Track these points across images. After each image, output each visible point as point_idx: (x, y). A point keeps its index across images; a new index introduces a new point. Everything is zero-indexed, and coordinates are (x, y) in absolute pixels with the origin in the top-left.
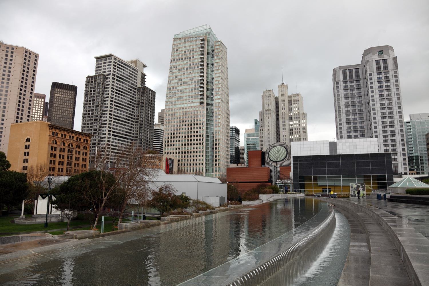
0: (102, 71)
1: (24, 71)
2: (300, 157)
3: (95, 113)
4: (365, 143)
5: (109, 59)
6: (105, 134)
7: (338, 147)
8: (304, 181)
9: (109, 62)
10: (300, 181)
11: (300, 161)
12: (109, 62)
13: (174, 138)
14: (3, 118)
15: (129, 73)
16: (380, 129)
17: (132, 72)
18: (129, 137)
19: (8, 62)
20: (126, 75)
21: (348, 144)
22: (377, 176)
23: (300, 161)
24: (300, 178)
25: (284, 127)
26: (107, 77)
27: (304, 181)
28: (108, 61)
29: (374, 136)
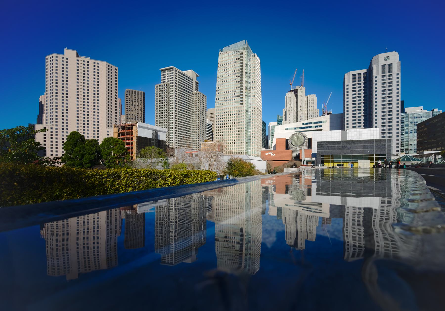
0: (167, 80)
1: (108, 78)
2: (322, 142)
3: (165, 103)
4: (369, 132)
5: (171, 71)
6: (173, 108)
7: (348, 135)
8: (323, 159)
9: (171, 73)
10: (322, 159)
11: (322, 145)
12: (171, 73)
13: (222, 124)
14: (78, 119)
15: (187, 82)
16: (380, 121)
17: (189, 80)
18: (184, 88)
19: (65, 76)
20: (185, 80)
21: (355, 133)
22: (379, 155)
23: (322, 145)
24: (322, 156)
25: (301, 118)
26: (171, 85)
27: (323, 159)
28: (170, 72)
29: (374, 127)
